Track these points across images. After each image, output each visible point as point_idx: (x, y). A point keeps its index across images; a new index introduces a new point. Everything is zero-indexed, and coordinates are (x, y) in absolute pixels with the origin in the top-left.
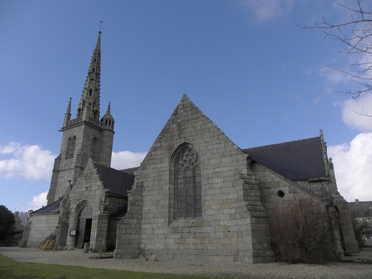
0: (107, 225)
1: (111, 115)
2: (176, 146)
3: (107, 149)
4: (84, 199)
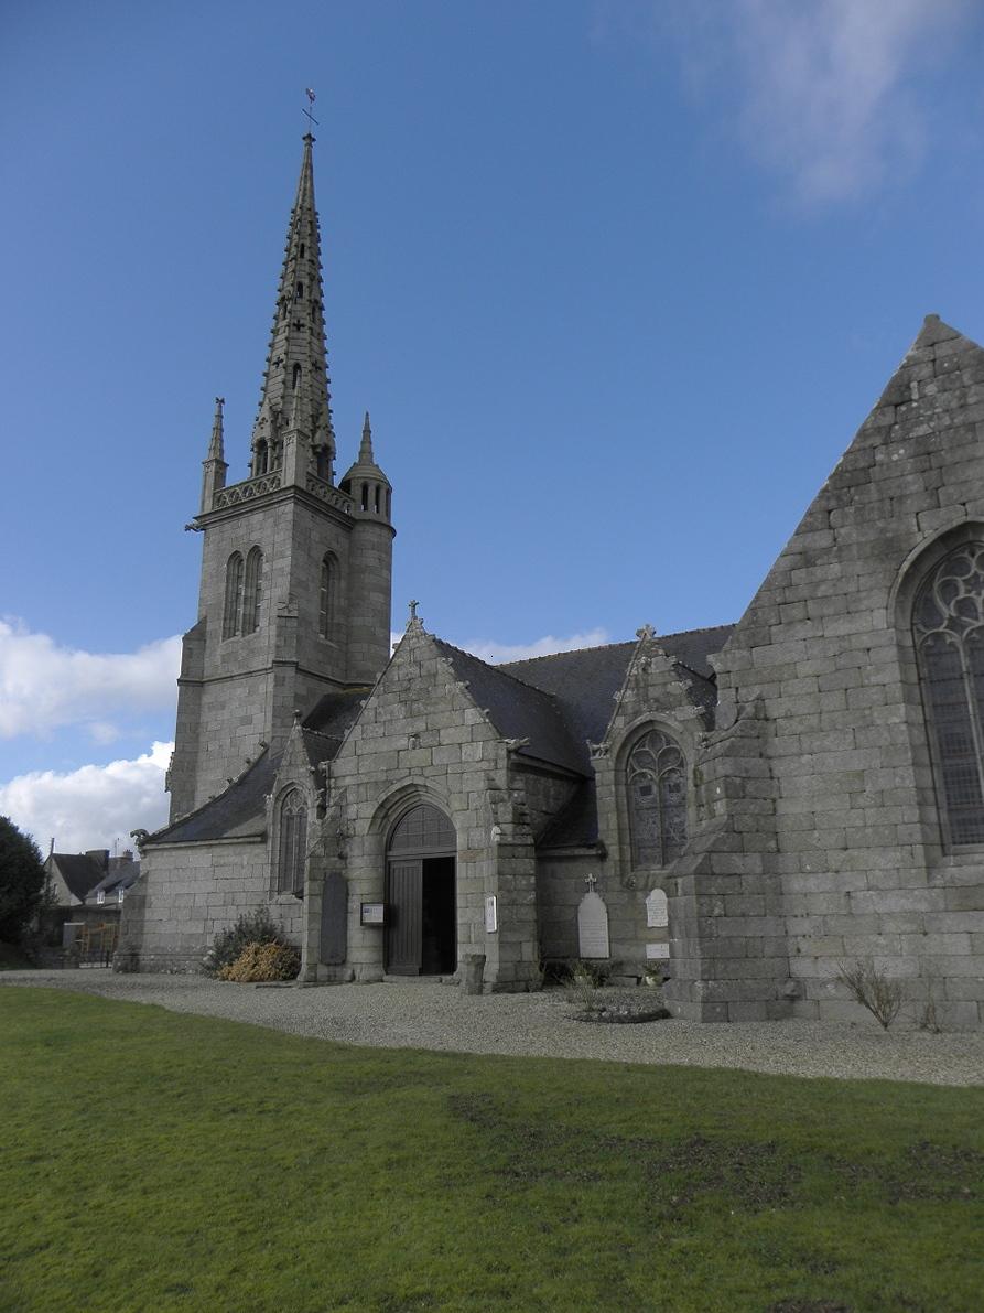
0: (533, 880)
1: (377, 466)
2: (921, 542)
3: (376, 597)
4: (407, 782)
